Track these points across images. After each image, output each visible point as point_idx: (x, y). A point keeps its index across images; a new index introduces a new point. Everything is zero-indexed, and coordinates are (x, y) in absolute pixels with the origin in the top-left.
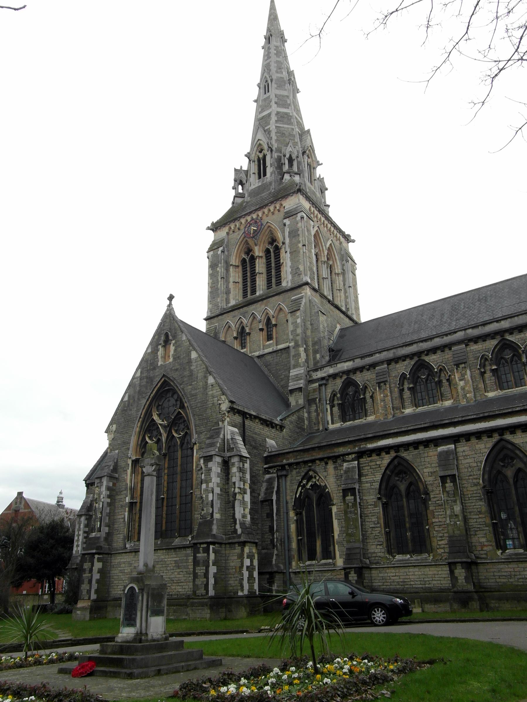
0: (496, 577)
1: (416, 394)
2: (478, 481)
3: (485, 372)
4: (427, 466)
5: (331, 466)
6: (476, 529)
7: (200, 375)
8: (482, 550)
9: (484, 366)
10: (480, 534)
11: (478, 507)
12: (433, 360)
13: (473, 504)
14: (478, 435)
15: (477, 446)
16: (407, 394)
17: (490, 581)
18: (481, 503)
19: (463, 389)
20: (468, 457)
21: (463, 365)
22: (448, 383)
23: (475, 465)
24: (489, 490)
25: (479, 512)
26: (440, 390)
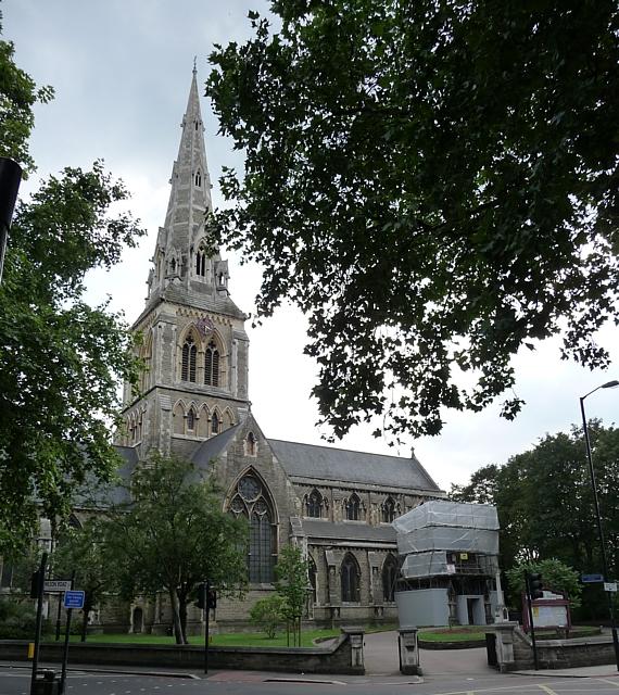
4: (361, 558)
7: (281, 477)
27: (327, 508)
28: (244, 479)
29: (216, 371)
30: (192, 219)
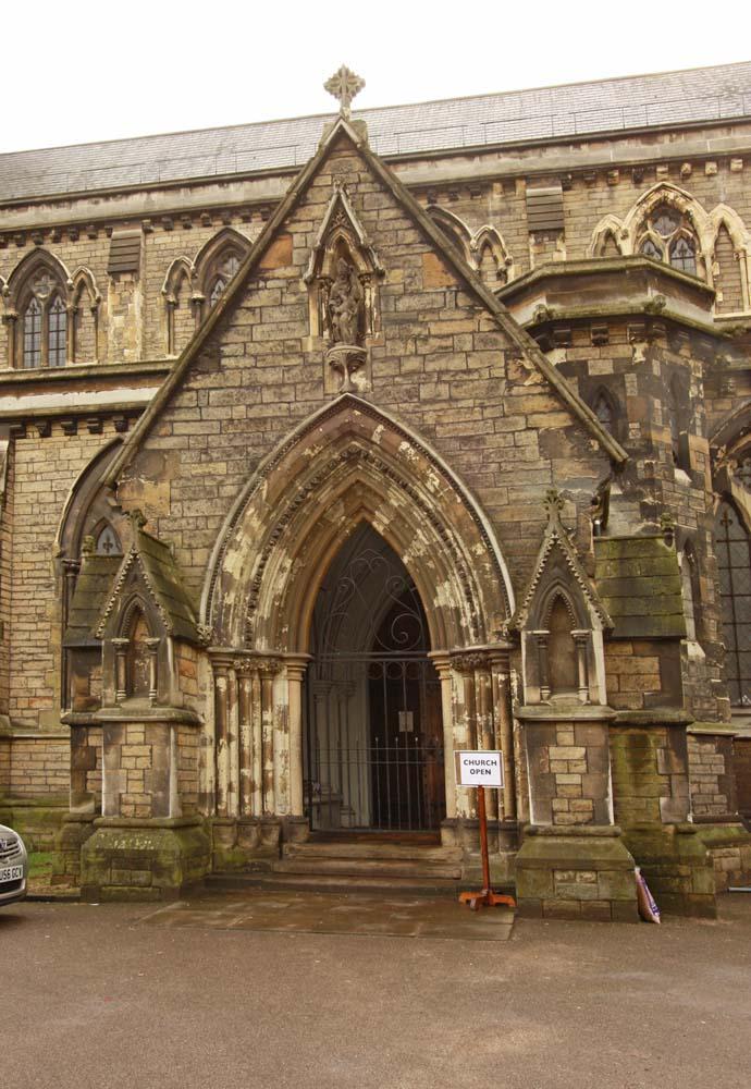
0: (50, 773)
1: (19, 336)
2: (50, 539)
3: (176, 305)
6: (25, 657)
8: (29, 708)
9: (178, 289)
10: (33, 669)
11: (37, 603)
12: (68, 255)
13: (30, 596)
14: (71, 421)
15: (64, 453)
17: (35, 781)
18: (47, 595)
19: (119, 335)
20: (39, 477)
21: (128, 278)
22: (93, 320)
23: (51, 498)
24: (70, 563)
25: (40, 615)
26: (74, 334)
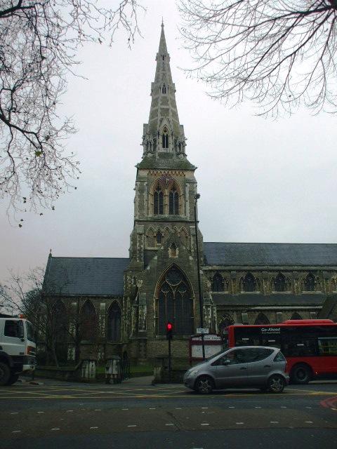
5: (235, 313)
14: (289, 310)
16: (242, 286)
27: (259, 284)
28: (170, 271)
29: (177, 205)
30: (159, 114)
